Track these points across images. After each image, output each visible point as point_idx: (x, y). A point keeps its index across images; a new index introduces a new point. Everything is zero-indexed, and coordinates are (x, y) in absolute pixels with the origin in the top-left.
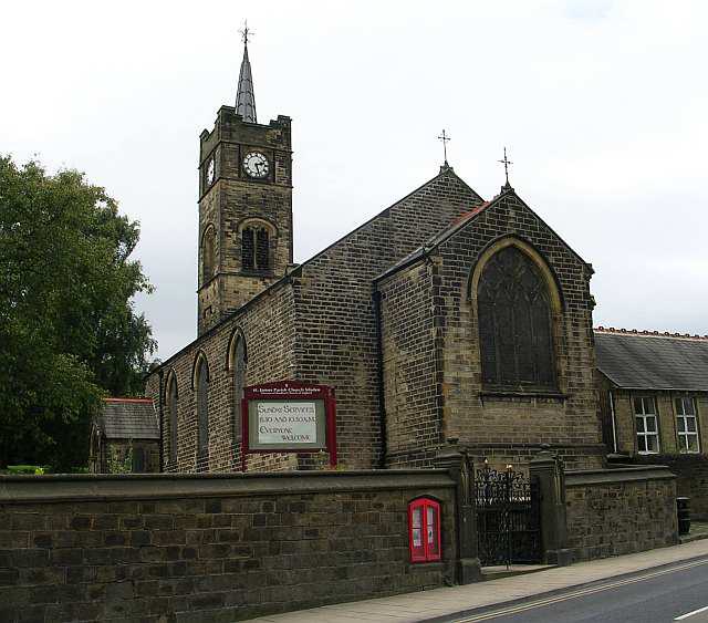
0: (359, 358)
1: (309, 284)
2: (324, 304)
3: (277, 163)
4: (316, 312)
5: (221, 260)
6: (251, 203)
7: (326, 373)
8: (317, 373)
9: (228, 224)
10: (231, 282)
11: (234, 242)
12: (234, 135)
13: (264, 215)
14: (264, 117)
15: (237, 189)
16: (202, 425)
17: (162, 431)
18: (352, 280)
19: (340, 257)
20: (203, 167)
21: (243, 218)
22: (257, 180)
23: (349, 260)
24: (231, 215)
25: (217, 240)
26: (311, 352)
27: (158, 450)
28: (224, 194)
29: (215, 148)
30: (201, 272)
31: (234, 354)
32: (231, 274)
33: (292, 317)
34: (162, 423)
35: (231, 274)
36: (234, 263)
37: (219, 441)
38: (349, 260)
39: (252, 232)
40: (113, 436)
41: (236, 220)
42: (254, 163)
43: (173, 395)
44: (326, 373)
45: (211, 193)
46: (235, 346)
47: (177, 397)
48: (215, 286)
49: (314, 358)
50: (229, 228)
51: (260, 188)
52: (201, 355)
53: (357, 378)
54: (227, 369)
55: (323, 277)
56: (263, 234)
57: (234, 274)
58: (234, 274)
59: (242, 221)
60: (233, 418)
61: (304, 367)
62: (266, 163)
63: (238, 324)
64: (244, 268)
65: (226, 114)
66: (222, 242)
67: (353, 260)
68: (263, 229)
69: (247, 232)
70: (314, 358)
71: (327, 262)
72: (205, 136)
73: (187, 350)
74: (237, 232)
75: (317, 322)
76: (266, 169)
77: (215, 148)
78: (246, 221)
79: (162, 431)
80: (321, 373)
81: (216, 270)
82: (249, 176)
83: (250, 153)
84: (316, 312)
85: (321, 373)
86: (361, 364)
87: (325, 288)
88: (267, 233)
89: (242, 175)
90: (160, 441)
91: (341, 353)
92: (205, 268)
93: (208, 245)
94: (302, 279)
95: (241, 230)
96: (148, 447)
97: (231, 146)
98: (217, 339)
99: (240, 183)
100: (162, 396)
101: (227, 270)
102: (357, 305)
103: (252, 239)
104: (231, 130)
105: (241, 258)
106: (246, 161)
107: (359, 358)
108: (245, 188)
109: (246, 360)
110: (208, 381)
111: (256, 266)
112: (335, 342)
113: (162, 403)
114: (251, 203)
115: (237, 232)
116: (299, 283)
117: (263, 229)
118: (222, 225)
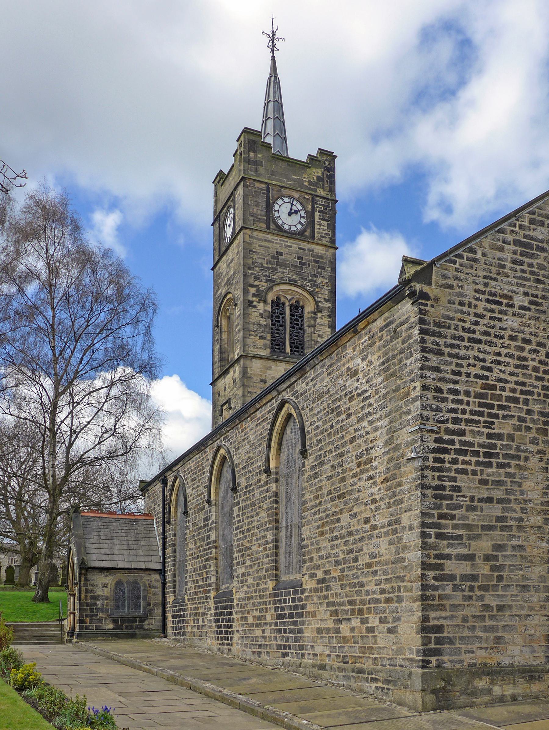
0: (530, 447)
1: (444, 301)
2: (470, 340)
3: (317, 215)
4: (456, 356)
5: (244, 338)
6: (284, 265)
7: (474, 473)
8: (458, 471)
9: (253, 290)
10: (256, 366)
11: (261, 315)
12: (261, 169)
13: (299, 283)
14: (299, 149)
15: (267, 244)
16: (224, 557)
17: (164, 558)
18: (519, 300)
19: (499, 254)
20: (214, 337)
21: (272, 283)
22: (291, 235)
23: (515, 262)
24: (257, 278)
25: (238, 311)
26: (448, 431)
27: (160, 585)
28: (248, 251)
29: (236, 188)
30: (217, 358)
31: (280, 444)
32: (257, 357)
33: (413, 363)
34: (164, 548)
35: (257, 357)
36: (261, 342)
37: (250, 581)
38: (515, 262)
39: (284, 304)
40: (97, 564)
41: (263, 285)
42: (288, 214)
43: (180, 510)
44: (474, 473)
45: (230, 252)
46: (220, 472)
47: (185, 513)
48: (236, 372)
49: (452, 442)
50: (254, 295)
51: (294, 245)
52: (222, 451)
53: (527, 485)
54: (267, 471)
55: (469, 290)
56: (297, 308)
57: (262, 358)
58: (262, 358)
59: (271, 288)
60: (277, 547)
61: (436, 460)
62: (303, 213)
63: (287, 395)
64: (273, 350)
65: (250, 140)
66: (245, 315)
67: (522, 263)
68: (298, 302)
69: (277, 304)
70: (452, 442)
71: (475, 260)
72: (221, 178)
73: (199, 447)
74: (265, 301)
75: (459, 374)
76: (303, 221)
77: (236, 188)
78: (276, 289)
79: (164, 558)
80: (465, 472)
81: (237, 352)
82: (280, 229)
83: (282, 196)
84: (456, 356)
85: (465, 472)
86: (534, 461)
87: (472, 310)
88: (303, 307)
89: (272, 226)
90: (162, 572)
91: (499, 437)
92: (221, 352)
93: (224, 323)
94: (432, 291)
95: (269, 301)
96: (146, 578)
97: (257, 185)
98: (249, 424)
99: (270, 237)
100: (166, 511)
101: (252, 351)
102: (528, 347)
103: (283, 313)
104: (256, 163)
105: (269, 337)
106: (276, 207)
107: (530, 447)
108: (277, 243)
109: (304, 453)
110: (234, 490)
111: (288, 349)
112: (490, 415)
113: (165, 522)
114: (284, 265)
115: (265, 301)
116: (424, 296)
117: (298, 302)
118: (245, 292)
